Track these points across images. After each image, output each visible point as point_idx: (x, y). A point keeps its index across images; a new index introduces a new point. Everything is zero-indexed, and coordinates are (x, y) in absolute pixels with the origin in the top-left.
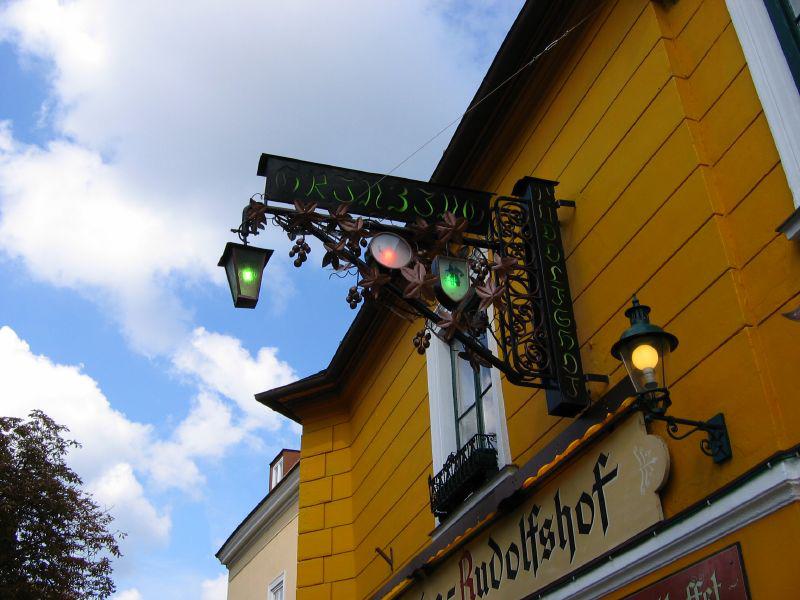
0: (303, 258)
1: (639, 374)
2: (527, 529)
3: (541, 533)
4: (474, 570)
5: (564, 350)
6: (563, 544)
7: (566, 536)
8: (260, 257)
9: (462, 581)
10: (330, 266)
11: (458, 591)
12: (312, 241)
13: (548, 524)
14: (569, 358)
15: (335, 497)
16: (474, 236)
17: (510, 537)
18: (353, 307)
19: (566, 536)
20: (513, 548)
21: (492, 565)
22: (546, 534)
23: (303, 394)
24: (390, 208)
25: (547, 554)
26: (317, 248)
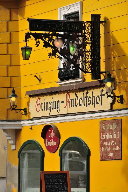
0: (38, 45)
1: (109, 88)
2: (85, 96)
3: (88, 98)
4: (70, 99)
5: (97, 41)
6: (93, 104)
7: (94, 103)
8: (30, 49)
9: (66, 100)
10: (45, 47)
11: (65, 102)
12: (40, 40)
13: (90, 97)
14: (97, 68)
15: (6, 66)
16: (84, 55)
17: (80, 95)
18: (84, 106)
19: (94, 103)
20: (81, 98)
21: (75, 100)
22: (89, 100)
23: (88, 119)
24: (59, 30)
25: (89, 104)
26: (42, 43)
